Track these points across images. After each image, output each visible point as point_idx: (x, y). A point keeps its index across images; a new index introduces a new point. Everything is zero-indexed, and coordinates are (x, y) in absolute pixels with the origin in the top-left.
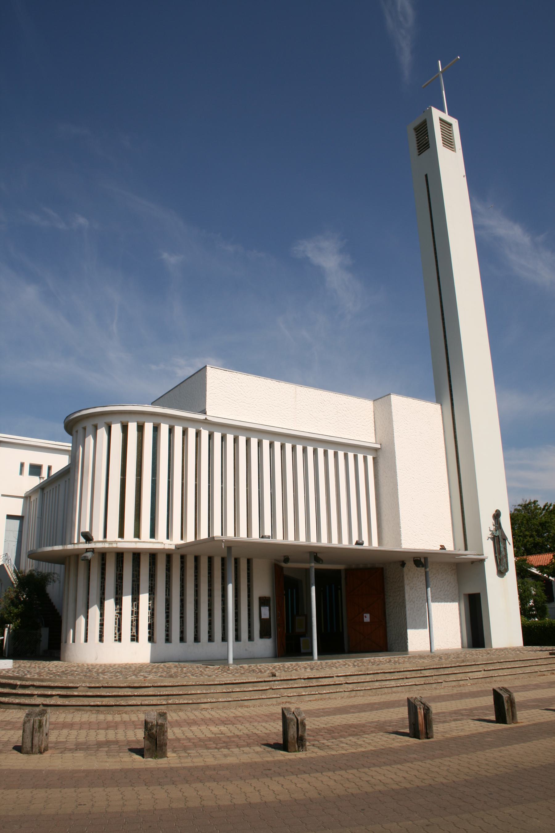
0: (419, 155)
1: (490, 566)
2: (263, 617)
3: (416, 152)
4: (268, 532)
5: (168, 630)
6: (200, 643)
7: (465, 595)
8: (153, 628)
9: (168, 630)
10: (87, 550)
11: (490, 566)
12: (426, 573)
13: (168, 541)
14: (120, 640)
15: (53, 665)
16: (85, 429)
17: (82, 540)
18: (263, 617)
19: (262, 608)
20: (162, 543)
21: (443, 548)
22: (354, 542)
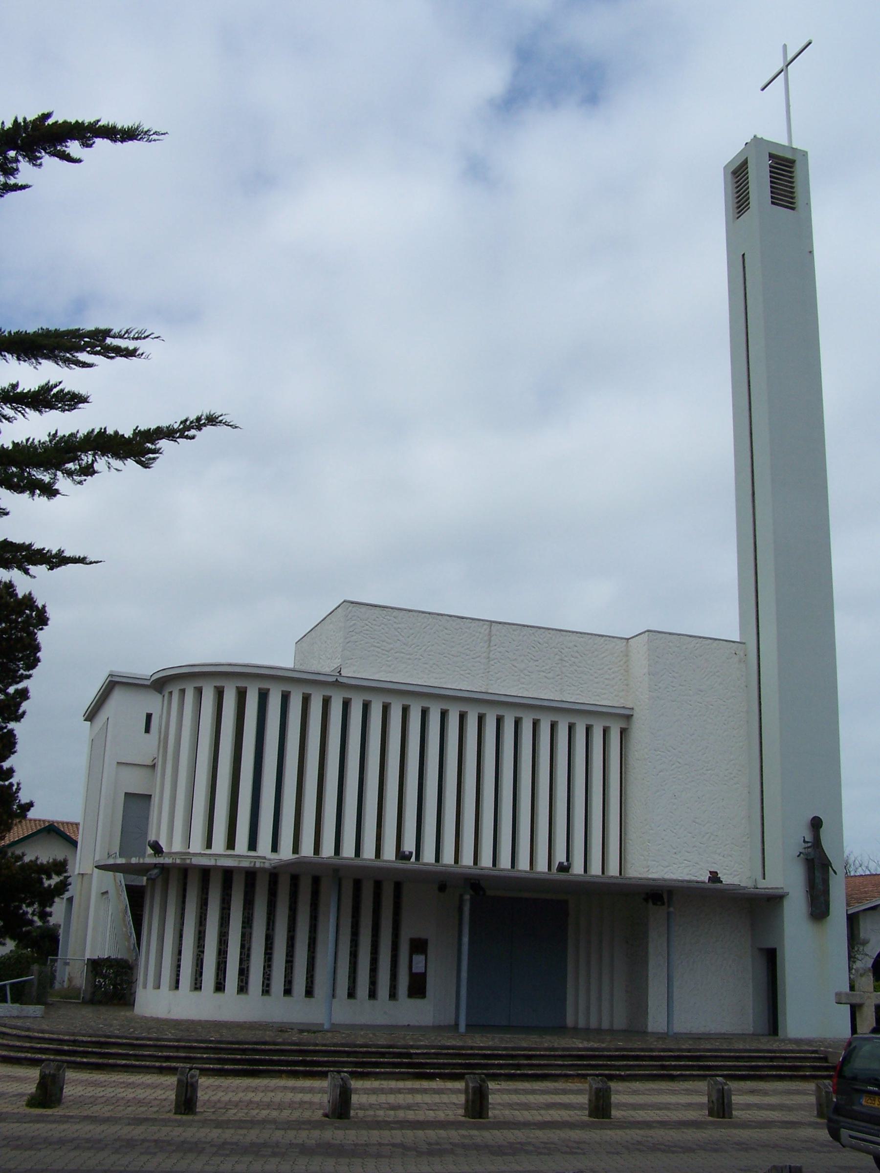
0: (83, 400)
1: (795, 907)
2: (414, 970)
3: (750, 164)
4: (409, 846)
5: (373, 983)
6: (312, 999)
7: (761, 950)
8: (248, 974)
9: (373, 983)
10: (155, 866)
11: (795, 907)
12: (669, 913)
13: (274, 856)
14: (177, 987)
15: (124, 1013)
16: (171, 693)
17: (150, 851)
18: (414, 970)
19: (414, 956)
20: (264, 858)
21: (714, 877)
22: (555, 866)
